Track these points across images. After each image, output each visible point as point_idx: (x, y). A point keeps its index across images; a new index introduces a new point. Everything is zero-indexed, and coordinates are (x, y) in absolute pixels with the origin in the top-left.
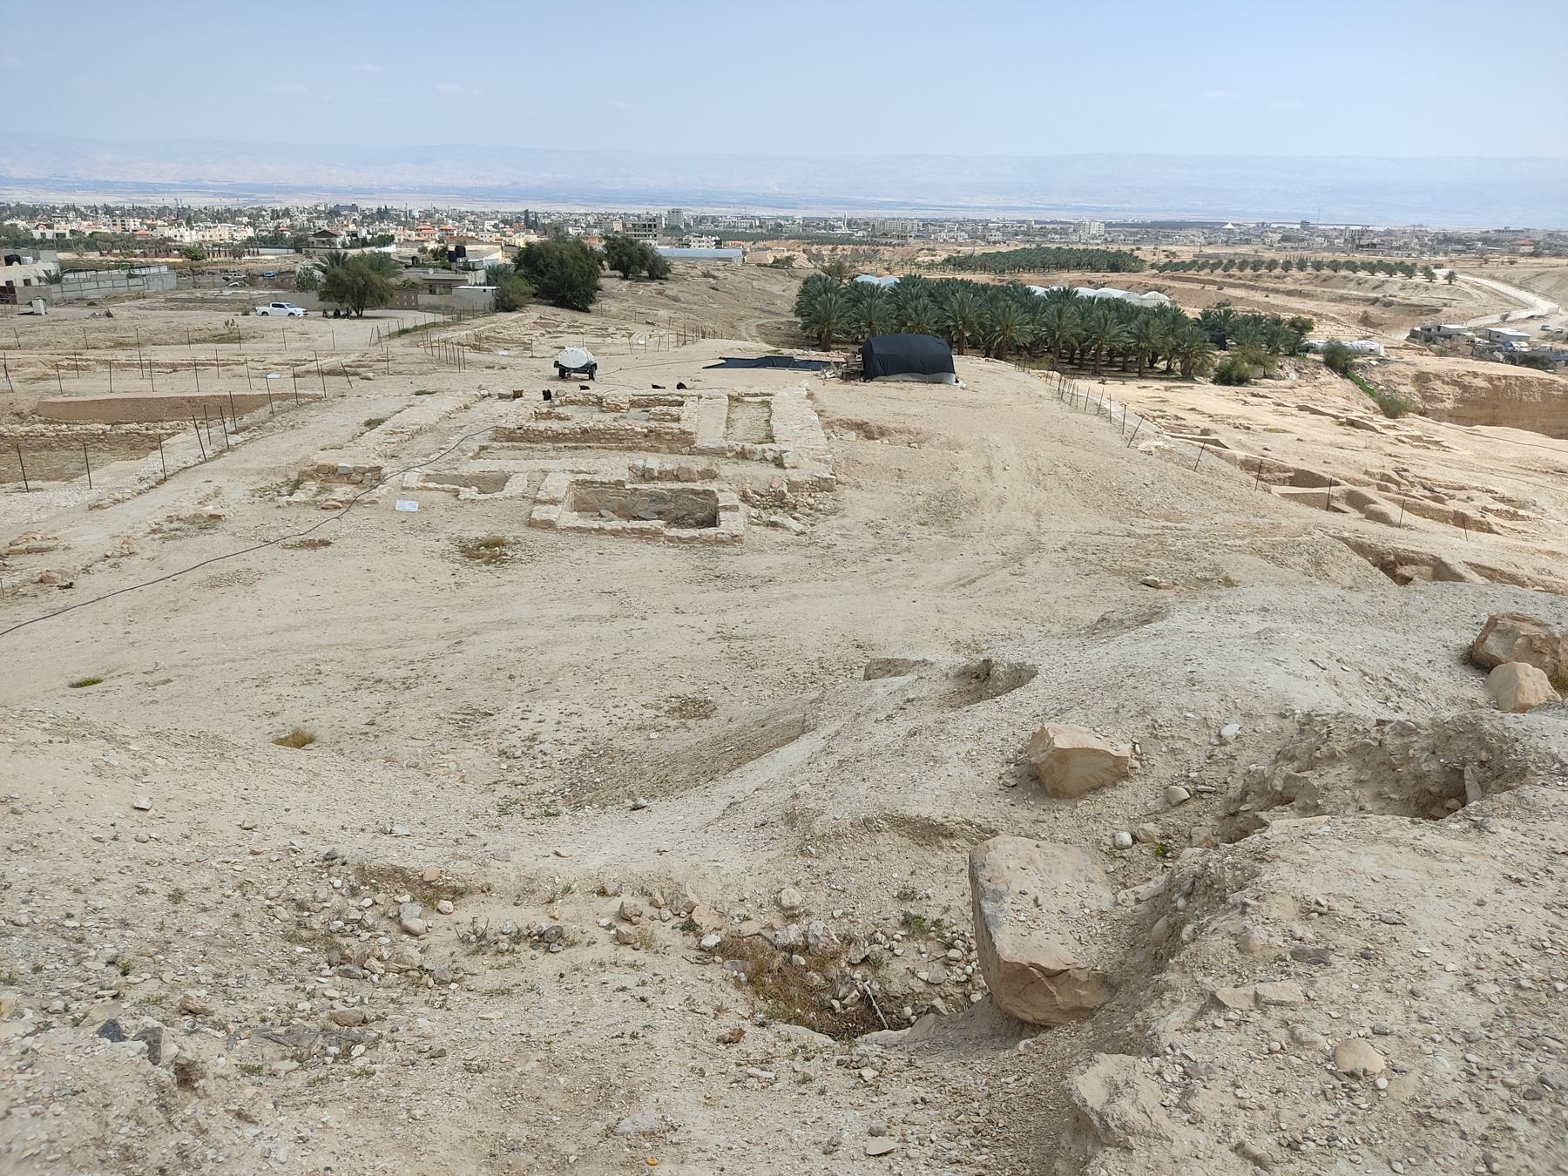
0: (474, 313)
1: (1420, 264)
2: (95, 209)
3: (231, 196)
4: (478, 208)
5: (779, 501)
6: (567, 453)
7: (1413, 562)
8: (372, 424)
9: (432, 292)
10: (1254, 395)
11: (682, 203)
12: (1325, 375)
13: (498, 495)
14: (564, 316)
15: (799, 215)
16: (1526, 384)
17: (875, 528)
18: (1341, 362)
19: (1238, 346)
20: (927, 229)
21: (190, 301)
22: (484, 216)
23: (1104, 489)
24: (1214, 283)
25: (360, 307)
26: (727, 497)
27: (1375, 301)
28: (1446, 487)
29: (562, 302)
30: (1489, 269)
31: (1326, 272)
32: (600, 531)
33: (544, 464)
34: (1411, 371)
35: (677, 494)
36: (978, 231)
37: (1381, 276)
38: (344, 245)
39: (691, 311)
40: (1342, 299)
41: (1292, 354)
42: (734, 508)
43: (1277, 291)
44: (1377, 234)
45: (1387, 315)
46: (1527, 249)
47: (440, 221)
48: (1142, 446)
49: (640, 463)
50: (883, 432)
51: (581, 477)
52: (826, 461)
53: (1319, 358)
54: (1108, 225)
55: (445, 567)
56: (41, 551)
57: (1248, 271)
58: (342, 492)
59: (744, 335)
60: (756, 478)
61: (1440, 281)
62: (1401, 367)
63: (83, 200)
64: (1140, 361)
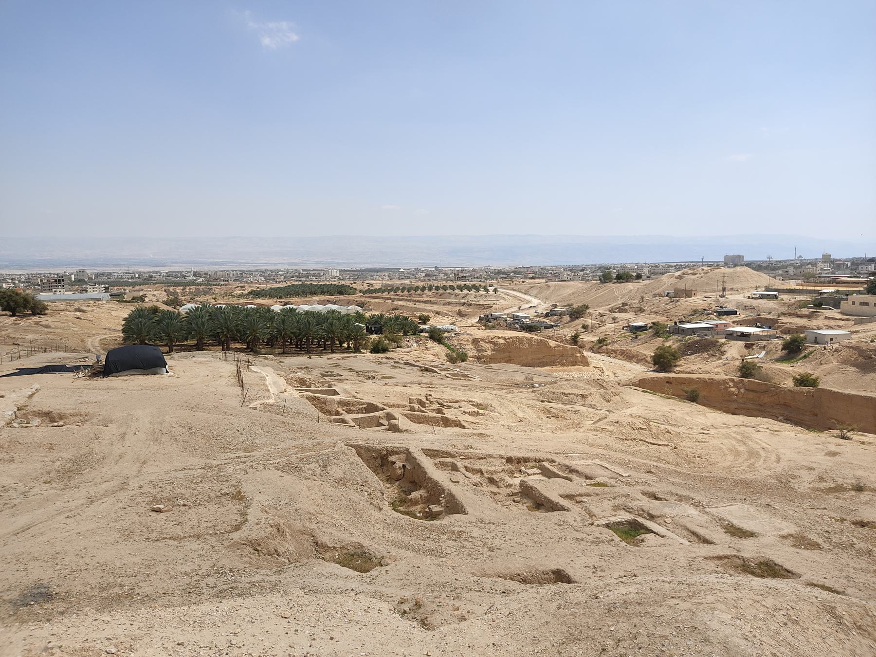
1: (483, 285)
7: (396, 453)
10: (387, 358)
11: (84, 266)
12: (430, 344)
15: (165, 270)
16: (521, 340)
18: (436, 336)
19: (382, 333)
20: (241, 276)
23: (206, 437)
24: (390, 299)
27: (464, 304)
28: (450, 402)
30: (513, 286)
31: (441, 291)
34: (470, 338)
36: (270, 275)
37: (465, 291)
40: (449, 304)
41: (414, 334)
43: (420, 302)
44: (469, 271)
45: (470, 310)
46: (531, 275)
48: (252, 406)
50: (61, 417)
53: (427, 335)
54: (341, 271)
57: (406, 292)
61: (491, 292)
62: (466, 336)
64: (333, 343)
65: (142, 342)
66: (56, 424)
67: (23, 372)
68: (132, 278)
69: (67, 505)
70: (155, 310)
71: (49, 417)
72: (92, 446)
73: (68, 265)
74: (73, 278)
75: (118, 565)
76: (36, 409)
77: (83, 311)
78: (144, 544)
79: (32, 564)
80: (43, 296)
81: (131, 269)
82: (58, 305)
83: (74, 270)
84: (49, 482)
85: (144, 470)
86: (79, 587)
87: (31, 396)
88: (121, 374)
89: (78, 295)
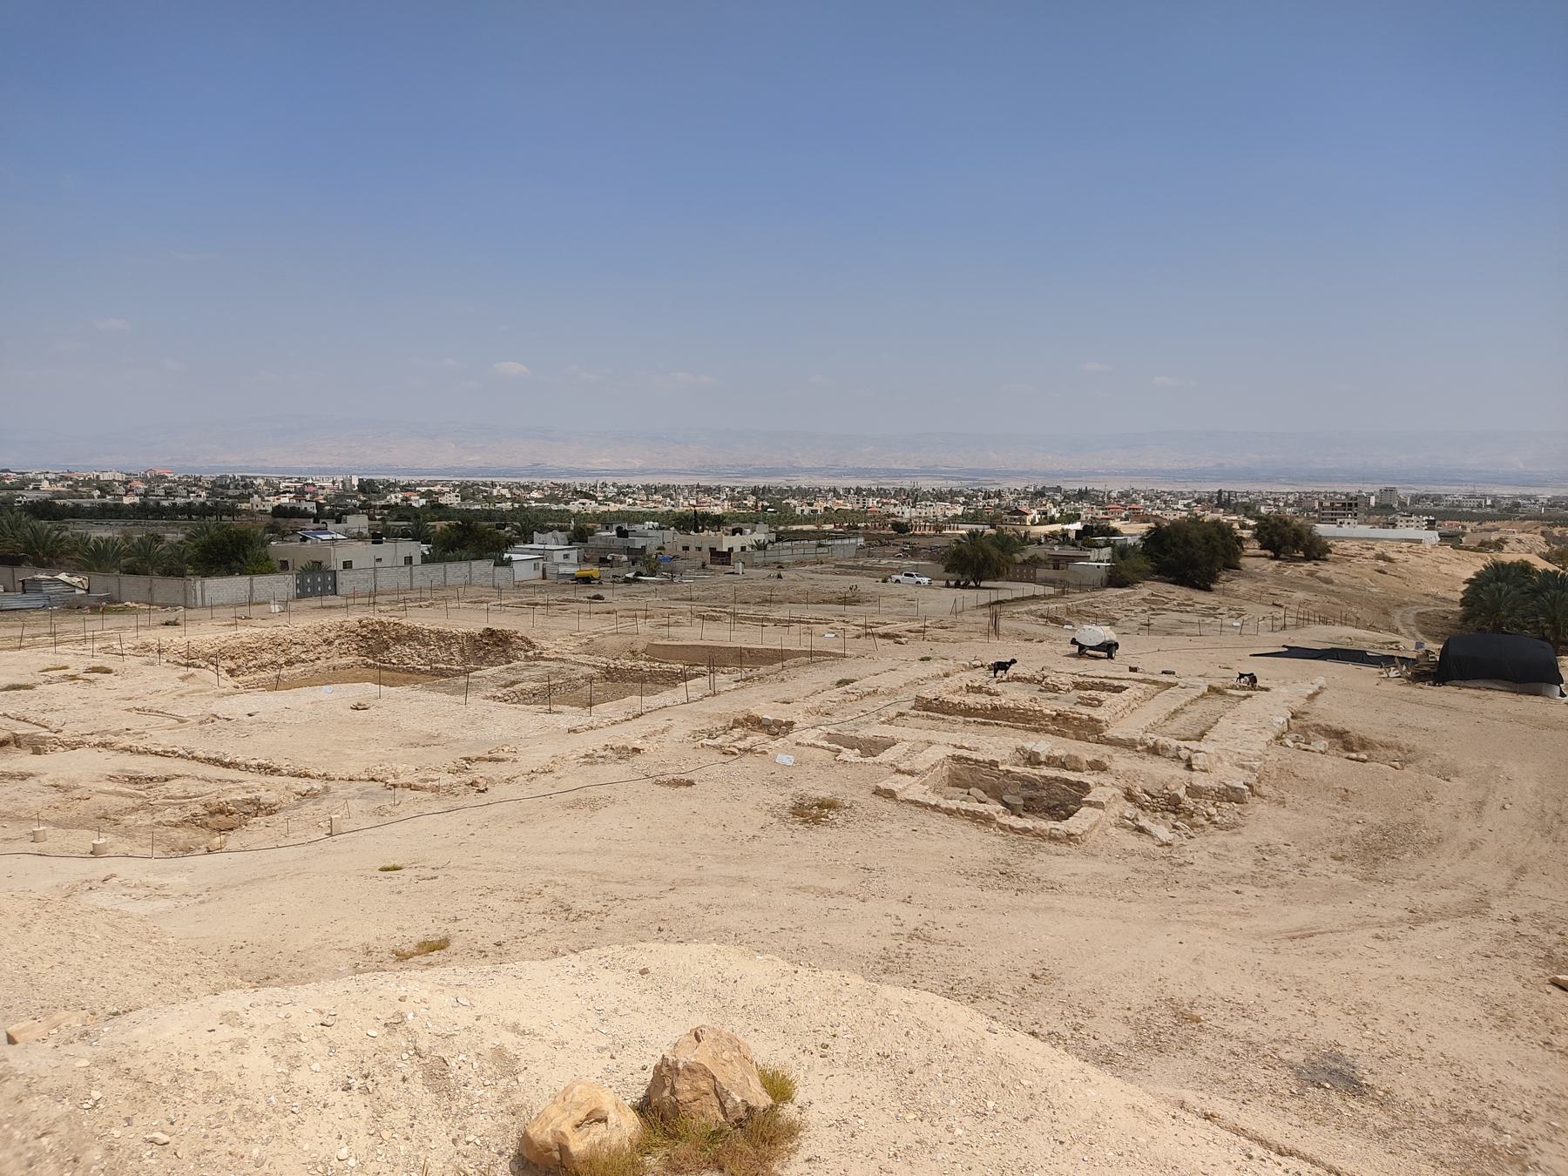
0: (1081, 587)
2: (848, 491)
3: (959, 479)
4: (1178, 488)
5: (1173, 805)
6: (973, 728)
8: (841, 683)
9: (1056, 567)
13: (870, 760)
14: (1180, 593)
15: (1545, 494)
17: (1264, 852)
21: (852, 567)
22: (1182, 495)
25: (978, 577)
26: (1103, 789)
29: (1182, 580)
32: (935, 808)
33: (934, 736)
35: (1050, 781)
38: (1033, 523)
39: (1338, 595)
42: (1098, 805)
47: (1134, 501)
49: (1029, 746)
50: (1364, 745)
51: (959, 752)
52: (1252, 769)
55: (761, 818)
56: (498, 760)
58: (757, 738)
59: (1397, 624)
60: (1151, 776)
63: (841, 483)
65: (1498, 629)
66: (1354, 755)
67: (1294, 652)
68: (1480, 506)
69: (1372, 911)
70: (1525, 568)
71: (1344, 740)
72: (1418, 810)
73: (1365, 480)
74: (1373, 501)
75: (1487, 1079)
76: (1323, 723)
77: (1390, 560)
78: (1539, 1053)
79: (1322, 1008)
80: (1322, 529)
81: (1479, 491)
82: (1347, 545)
83: (1376, 488)
84: (1340, 859)
85: (1520, 885)
86: (1409, 1093)
87: (1312, 697)
88: (1467, 683)
89: (1379, 532)
